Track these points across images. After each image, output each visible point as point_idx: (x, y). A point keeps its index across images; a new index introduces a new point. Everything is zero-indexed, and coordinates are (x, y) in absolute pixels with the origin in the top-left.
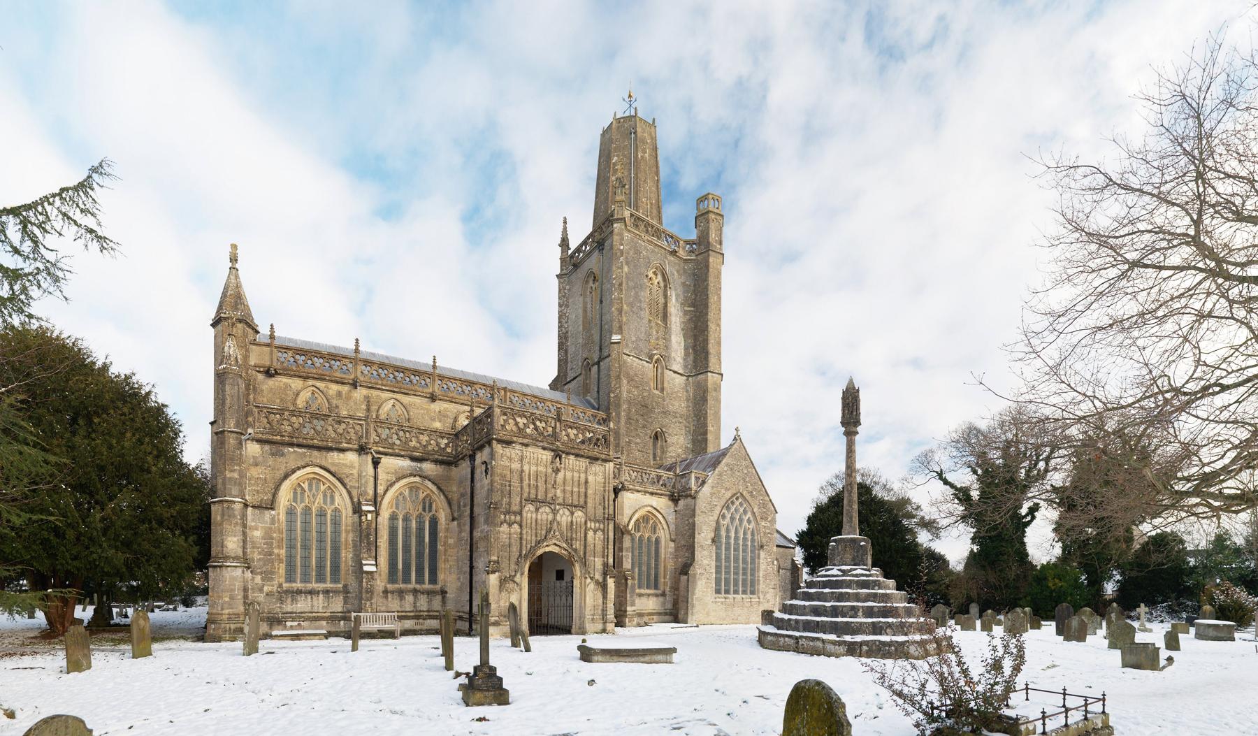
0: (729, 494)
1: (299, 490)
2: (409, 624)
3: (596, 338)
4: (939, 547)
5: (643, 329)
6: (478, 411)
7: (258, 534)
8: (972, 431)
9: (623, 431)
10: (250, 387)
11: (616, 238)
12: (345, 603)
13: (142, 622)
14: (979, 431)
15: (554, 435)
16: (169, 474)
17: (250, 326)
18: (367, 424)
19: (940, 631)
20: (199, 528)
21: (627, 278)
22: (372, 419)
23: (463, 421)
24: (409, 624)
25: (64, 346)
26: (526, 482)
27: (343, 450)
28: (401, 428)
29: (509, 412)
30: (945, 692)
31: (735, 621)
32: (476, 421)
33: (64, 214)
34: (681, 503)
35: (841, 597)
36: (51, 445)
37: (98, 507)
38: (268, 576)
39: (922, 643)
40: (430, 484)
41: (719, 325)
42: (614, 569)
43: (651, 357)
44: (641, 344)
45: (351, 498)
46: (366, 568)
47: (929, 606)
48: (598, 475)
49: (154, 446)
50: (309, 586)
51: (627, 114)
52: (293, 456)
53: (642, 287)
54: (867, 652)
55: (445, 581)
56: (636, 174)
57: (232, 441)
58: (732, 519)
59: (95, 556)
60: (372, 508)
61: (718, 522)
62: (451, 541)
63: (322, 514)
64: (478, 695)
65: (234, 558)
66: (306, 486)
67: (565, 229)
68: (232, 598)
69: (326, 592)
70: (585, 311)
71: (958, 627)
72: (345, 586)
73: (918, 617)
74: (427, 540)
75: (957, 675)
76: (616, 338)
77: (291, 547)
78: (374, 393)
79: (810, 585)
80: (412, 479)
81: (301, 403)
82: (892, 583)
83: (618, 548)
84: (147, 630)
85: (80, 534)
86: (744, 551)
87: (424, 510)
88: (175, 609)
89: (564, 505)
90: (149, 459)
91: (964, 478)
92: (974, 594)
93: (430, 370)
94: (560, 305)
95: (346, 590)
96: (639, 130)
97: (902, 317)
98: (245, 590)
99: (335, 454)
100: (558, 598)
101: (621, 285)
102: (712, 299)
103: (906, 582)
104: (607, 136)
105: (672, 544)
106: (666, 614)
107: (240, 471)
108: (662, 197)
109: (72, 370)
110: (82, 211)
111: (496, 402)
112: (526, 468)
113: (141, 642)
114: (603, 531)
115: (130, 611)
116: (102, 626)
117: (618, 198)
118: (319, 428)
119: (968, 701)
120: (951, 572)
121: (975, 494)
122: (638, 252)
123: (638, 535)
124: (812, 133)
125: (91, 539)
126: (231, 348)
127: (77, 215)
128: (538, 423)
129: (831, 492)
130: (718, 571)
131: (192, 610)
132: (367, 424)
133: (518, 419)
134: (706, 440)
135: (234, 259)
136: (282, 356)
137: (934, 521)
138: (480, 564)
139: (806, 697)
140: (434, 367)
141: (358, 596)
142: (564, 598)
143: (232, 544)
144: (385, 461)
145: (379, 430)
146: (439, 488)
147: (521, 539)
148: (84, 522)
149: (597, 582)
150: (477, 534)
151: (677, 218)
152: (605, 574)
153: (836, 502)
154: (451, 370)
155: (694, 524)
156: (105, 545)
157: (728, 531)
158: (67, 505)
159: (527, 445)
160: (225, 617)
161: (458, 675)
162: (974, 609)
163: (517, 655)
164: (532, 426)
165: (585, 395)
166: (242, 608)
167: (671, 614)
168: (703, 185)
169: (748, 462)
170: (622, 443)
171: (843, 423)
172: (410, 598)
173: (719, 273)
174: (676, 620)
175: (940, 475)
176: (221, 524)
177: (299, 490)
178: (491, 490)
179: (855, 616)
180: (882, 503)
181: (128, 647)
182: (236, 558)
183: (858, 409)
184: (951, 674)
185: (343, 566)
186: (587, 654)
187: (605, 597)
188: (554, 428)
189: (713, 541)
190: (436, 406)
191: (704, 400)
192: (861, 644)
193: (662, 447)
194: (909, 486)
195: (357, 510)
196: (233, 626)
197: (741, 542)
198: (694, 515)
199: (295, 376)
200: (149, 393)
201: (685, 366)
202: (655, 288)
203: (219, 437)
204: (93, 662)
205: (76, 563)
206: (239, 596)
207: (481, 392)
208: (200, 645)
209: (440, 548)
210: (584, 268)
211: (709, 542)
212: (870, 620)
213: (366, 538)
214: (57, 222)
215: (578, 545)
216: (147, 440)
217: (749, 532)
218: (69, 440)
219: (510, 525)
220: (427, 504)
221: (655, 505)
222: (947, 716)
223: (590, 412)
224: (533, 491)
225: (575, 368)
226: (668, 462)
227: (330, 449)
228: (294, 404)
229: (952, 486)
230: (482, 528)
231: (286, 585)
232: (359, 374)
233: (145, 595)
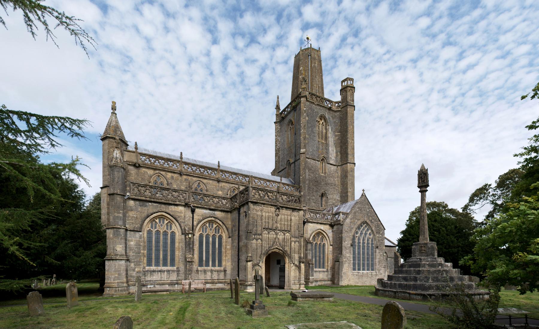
0: (359, 222)
3: (293, 151)
5: (315, 146)
11: (302, 105)
12: (178, 276)
27: (177, 205)
34: (335, 227)
41: (353, 140)
45: (181, 227)
48: (296, 217)
50: (160, 268)
52: (151, 207)
58: (361, 234)
61: (354, 236)
63: (165, 233)
67: (278, 101)
69: (168, 271)
72: (177, 268)
76: (302, 151)
77: (150, 250)
80: (210, 219)
82: (449, 264)
86: (368, 249)
93: (217, 168)
95: (178, 271)
97: (427, 149)
98: (127, 271)
99: (173, 207)
105: (331, 247)
114: (299, 242)
123: (314, 243)
134: (347, 196)
138: (243, 258)
147: (262, 246)
149: (296, 266)
150: (241, 244)
151: (332, 93)
152: (300, 262)
155: (342, 237)
157: (359, 239)
172: (209, 274)
173: (353, 115)
178: (248, 225)
187: (300, 272)
188: (276, 196)
189: (352, 245)
191: (346, 176)
193: (325, 200)
197: (366, 245)
198: (341, 233)
201: (337, 161)
209: (223, 250)
211: (349, 245)
215: (287, 248)
217: (370, 240)
219: (257, 240)
221: (322, 228)
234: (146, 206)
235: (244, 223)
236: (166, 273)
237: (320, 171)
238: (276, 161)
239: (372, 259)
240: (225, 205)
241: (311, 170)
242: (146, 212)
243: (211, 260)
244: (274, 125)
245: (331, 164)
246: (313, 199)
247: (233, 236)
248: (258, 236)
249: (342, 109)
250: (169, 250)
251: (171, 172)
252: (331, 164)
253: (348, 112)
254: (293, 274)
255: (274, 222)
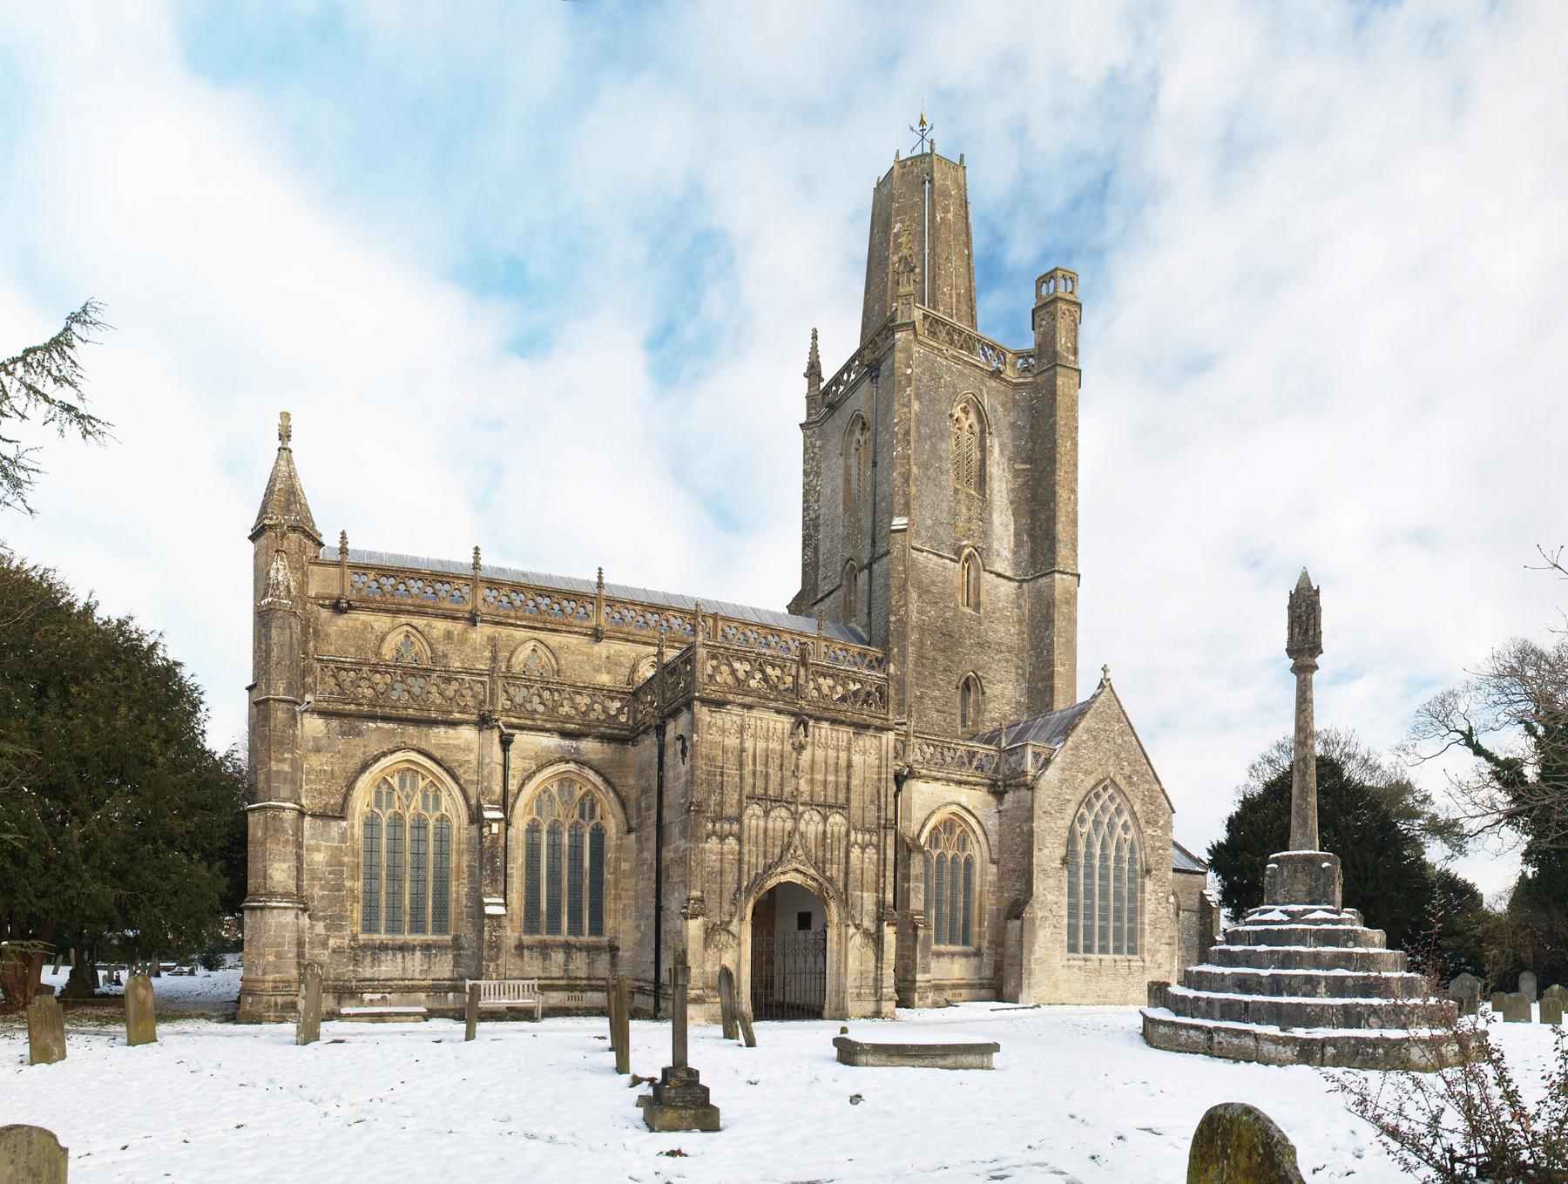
1: (384, 789)
2: (556, 998)
3: (866, 523)
4: (1465, 869)
5: (945, 505)
6: (671, 654)
7: (319, 857)
8: (1528, 654)
9: (910, 678)
10: (310, 630)
11: (899, 356)
12: (456, 964)
13: (141, 992)
14: (1541, 656)
15: (796, 690)
16: (183, 767)
17: (309, 536)
18: (493, 681)
19: (1466, 1022)
20: (229, 849)
21: (919, 421)
22: (500, 673)
23: (647, 671)
24: (556, 998)
25: (28, 581)
26: (748, 768)
27: (454, 724)
28: (546, 685)
29: (721, 654)
30: (1475, 1131)
31: (1102, 1000)
32: (666, 670)
33: (30, 387)
34: (1009, 797)
35: (1287, 960)
36: (7, 728)
37: (76, 820)
38: (335, 923)
39: (1433, 1043)
40: (592, 775)
41: (1074, 491)
42: (895, 911)
43: (958, 551)
44: (940, 530)
45: (467, 799)
46: (489, 910)
47: (1445, 979)
48: (868, 755)
49: (162, 725)
51: (918, 152)
52: (374, 736)
53: (943, 435)
54: (1334, 1056)
55: (616, 930)
56: (933, 249)
57: (280, 714)
58: (1097, 823)
59: (71, 892)
60: (499, 815)
61: (1072, 830)
62: (625, 866)
63: (420, 825)
64: (670, 1115)
65: (283, 895)
66: (395, 782)
67: (814, 348)
68: (279, 956)
69: (426, 947)
70: (847, 480)
71: (1499, 1016)
72: (456, 939)
73: (1426, 996)
74: (587, 864)
75: (1496, 1102)
76: (899, 522)
77: (372, 877)
78: (504, 631)
79: (1232, 938)
80: (563, 767)
81: (388, 652)
82: (1378, 935)
83: (902, 865)
84: (150, 1003)
85: (50, 860)
86: (1117, 879)
87: (582, 816)
88: (192, 973)
89: (811, 804)
90: (154, 745)
91: (1513, 742)
92: (1527, 954)
93: (593, 590)
94: (806, 474)
95: (457, 945)
96: (937, 176)
98: (300, 944)
99: (442, 730)
100: (801, 960)
101: (907, 433)
102: (1063, 447)
103: (1404, 934)
104: (885, 191)
105: (993, 869)
106: (981, 986)
107: (293, 761)
108: (975, 284)
109: (39, 616)
110: (56, 380)
111: (700, 638)
112: (749, 744)
113: (141, 1021)
114: (877, 847)
115: (124, 975)
116: (83, 999)
117: (902, 291)
118: (416, 690)
119: (1518, 1149)
120: (1486, 916)
121: (1531, 773)
122: (936, 377)
124: (1236, 148)
125: (65, 867)
126: (280, 571)
127: (49, 388)
128: (769, 670)
129: (1270, 775)
130: (1072, 914)
131: (218, 975)
132: (493, 681)
133: (737, 665)
134: (1052, 689)
135: (285, 435)
136: (360, 580)
137: (1455, 823)
138: (673, 904)
139: (1227, 1133)
140: (600, 585)
141: (476, 953)
142: (811, 959)
143: (280, 873)
144: (520, 738)
145: (511, 690)
146: (607, 781)
147: (740, 861)
148: (55, 841)
149: (866, 933)
150: (668, 854)
151: (1003, 316)
153: (1278, 790)
154: (627, 589)
155: (1031, 833)
156: (86, 876)
157: (1089, 844)
158: (31, 817)
159: (750, 707)
160: (269, 986)
161: (636, 1081)
162: (1528, 982)
163: (733, 1051)
164: (758, 676)
165: (847, 620)
166: (295, 972)
167: (990, 987)
168: (1046, 257)
169: (1124, 725)
170: (910, 699)
171: (1290, 652)
172: (558, 957)
173: (1075, 402)
174: (999, 997)
175: (1468, 738)
176: (263, 843)
177: (384, 789)
178: (691, 782)
179: (1313, 994)
180: (1360, 791)
181: (121, 1029)
182: (285, 895)
183: (1317, 624)
184: (1486, 1099)
185: (452, 906)
186: (848, 1052)
187: (879, 957)
189: (1064, 861)
190: (603, 649)
191: (1049, 620)
192: (1324, 1043)
193: (977, 702)
194: (1410, 759)
195: (476, 817)
196: (280, 1000)
197: (1111, 863)
198: (1031, 818)
199: (379, 610)
200: (153, 647)
201: (1017, 564)
202: (966, 434)
203: (260, 708)
204: (68, 1049)
205: (43, 903)
206: (292, 955)
207: (675, 622)
208: (230, 1027)
209: (608, 877)
210: (848, 410)
212: (1339, 1001)
213: (489, 861)
214: (19, 399)
215: (834, 871)
216: (150, 716)
218: (34, 720)
219: (722, 838)
220: (588, 807)
221: (964, 801)
222: (1479, 1174)
223: (856, 648)
224: (760, 783)
225: (830, 576)
226: (987, 728)
227: (434, 723)
228: (378, 654)
229: (1489, 757)
230: (676, 844)
231: (362, 937)
232: (480, 602)
233: (148, 951)
234: (359, 734)
235: (677, 778)
236: (418, 953)
237: (960, 598)
238: (804, 565)
239: (1132, 911)
240: (616, 717)
241: (927, 592)
242: (360, 753)
243: (565, 910)
244: (800, 434)
245: (999, 575)
246: (934, 699)
247: (640, 825)
248: (727, 826)
249: (1039, 379)
250: (430, 878)
251: (446, 617)
252: (999, 575)
253: (1059, 391)
254: (853, 964)
255: (788, 774)
